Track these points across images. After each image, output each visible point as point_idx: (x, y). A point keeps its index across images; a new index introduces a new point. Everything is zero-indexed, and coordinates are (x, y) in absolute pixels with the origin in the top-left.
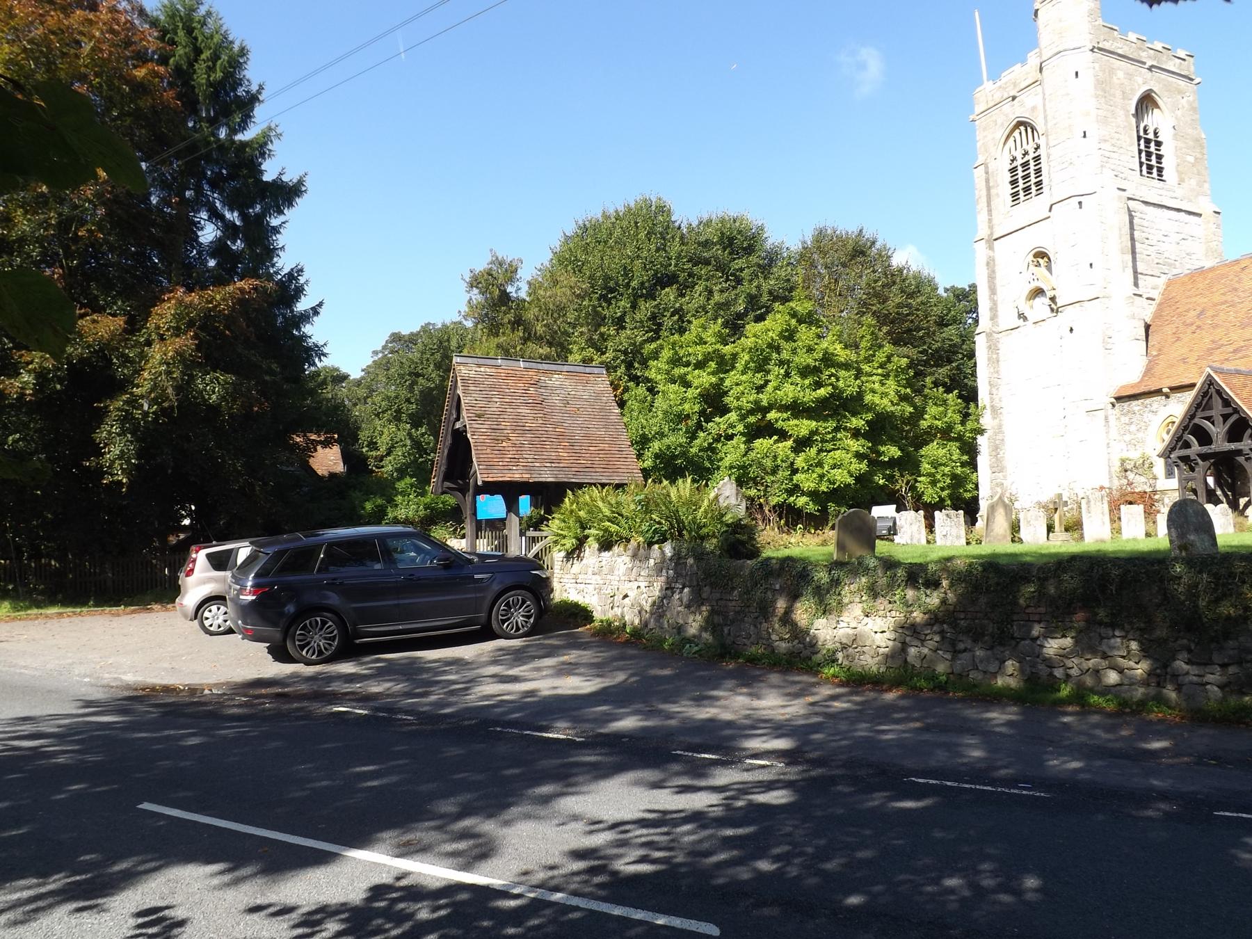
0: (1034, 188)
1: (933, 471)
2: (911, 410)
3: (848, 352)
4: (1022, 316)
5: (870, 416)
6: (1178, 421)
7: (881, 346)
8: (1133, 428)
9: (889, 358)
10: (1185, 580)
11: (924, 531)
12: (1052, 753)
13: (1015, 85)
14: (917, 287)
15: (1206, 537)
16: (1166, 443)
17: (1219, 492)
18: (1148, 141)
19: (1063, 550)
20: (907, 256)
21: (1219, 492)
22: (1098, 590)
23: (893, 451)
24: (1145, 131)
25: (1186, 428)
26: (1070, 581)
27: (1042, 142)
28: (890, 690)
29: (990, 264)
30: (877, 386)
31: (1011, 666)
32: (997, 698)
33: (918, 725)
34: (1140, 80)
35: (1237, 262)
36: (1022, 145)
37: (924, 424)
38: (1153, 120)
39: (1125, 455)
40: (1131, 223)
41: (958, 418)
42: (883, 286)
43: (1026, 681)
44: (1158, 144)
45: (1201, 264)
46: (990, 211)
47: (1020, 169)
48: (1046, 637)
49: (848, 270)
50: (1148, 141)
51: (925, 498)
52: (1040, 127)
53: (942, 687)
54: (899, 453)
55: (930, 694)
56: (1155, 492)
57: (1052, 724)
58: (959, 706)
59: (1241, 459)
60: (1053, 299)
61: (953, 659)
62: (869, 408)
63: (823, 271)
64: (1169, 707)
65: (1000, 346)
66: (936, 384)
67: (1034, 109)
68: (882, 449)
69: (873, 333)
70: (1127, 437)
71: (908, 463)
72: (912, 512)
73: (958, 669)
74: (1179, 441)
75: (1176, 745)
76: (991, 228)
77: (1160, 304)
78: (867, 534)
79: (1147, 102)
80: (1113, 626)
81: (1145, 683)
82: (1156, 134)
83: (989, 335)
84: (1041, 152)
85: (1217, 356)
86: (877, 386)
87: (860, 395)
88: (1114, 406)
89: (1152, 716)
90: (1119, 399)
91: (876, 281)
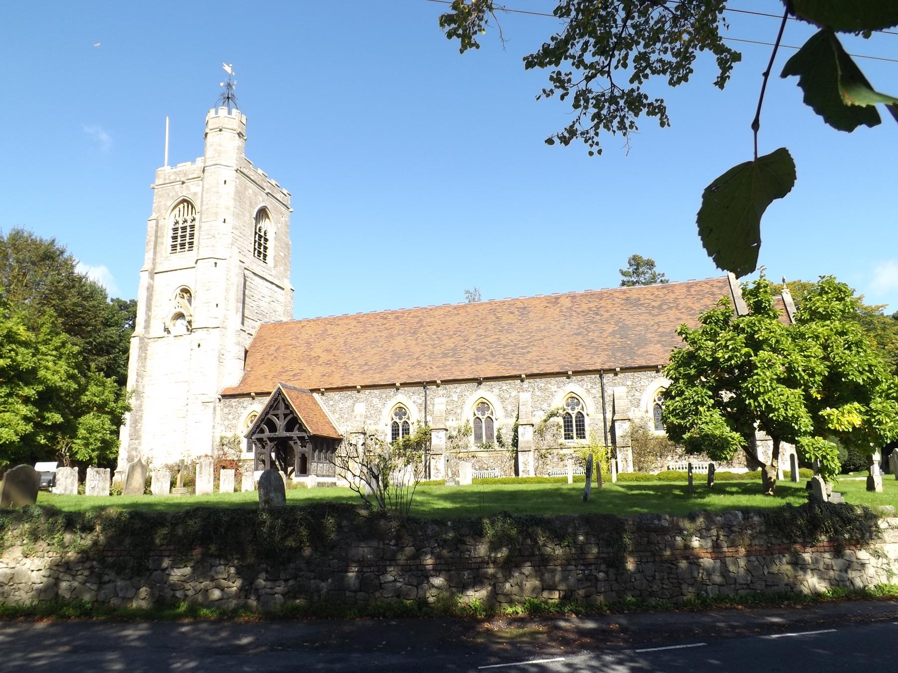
0: (187, 246)
1: (88, 435)
2: (76, 386)
3: (29, 333)
4: (167, 330)
5: (41, 388)
6: (258, 415)
7: (58, 334)
8: (230, 417)
9: (64, 344)
10: (268, 523)
11: (76, 483)
12: (175, 657)
13: (185, 174)
14: (91, 293)
15: (280, 495)
16: (250, 429)
17: (277, 463)
18: (260, 237)
19: (183, 500)
20: (92, 271)
21: (277, 463)
22: (210, 530)
23: (56, 418)
24: (260, 230)
25: (263, 420)
26: (194, 524)
27: (197, 217)
28: (41, 619)
29: (150, 289)
30: (50, 364)
31: (144, 591)
32: (132, 618)
33: (66, 648)
34: (261, 199)
35: (300, 322)
36: (182, 215)
37: (85, 399)
38: (265, 225)
39: (224, 434)
40: (245, 284)
41: (112, 397)
42: (65, 287)
43: (154, 602)
44: (266, 240)
45: (281, 319)
46: (155, 253)
47: (180, 230)
48: (172, 568)
49: (36, 268)
50: (260, 237)
51: (78, 456)
52: (197, 206)
53: (86, 613)
54: (62, 420)
55: (77, 620)
56: (239, 461)
57: (173, 634)
58: (101, 628)
59: (291, 443)
60: (190, 322)
61: (99, 590)
62: (41, 382)
63: (14, 264)
64: (252, 612)
65: (148, 348)
66: (100, 370)
67: (195, 194)
68: (47, 415)
69: (53, 323)
70: (226, 423)
71: (69, 429)
72: (69, 468)
73: (101, 597)
74: (257, 429)
75: (257, 639)
76: (154, 264)
77: (255, 339)
78: (31, 486)
79: (262, 213)
80: (219, 557)
81: (237, 596)
82: (265, 233)
83: (142, 339)
84: (196, 223)
85: (284, 377)
86: (50, 364)
87: (34, 371)
88: (220, 400)
89: (241, 619)
90: (224, 396)
91: (59, 282)
